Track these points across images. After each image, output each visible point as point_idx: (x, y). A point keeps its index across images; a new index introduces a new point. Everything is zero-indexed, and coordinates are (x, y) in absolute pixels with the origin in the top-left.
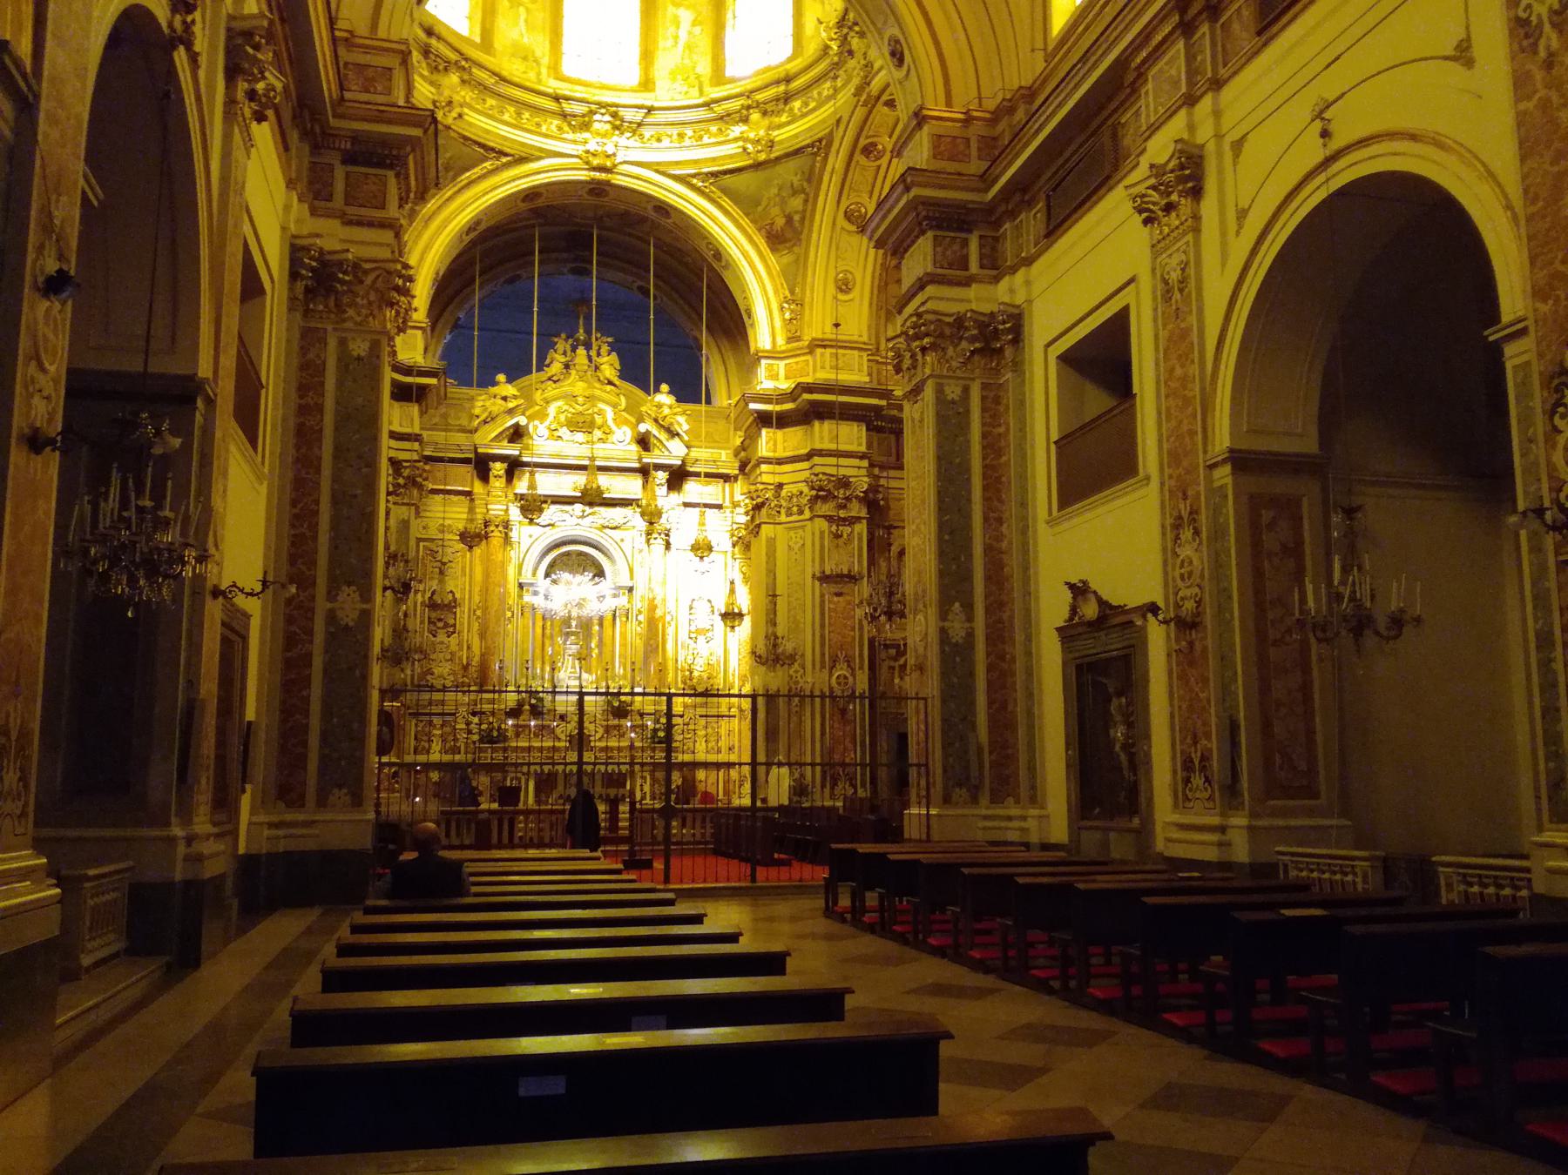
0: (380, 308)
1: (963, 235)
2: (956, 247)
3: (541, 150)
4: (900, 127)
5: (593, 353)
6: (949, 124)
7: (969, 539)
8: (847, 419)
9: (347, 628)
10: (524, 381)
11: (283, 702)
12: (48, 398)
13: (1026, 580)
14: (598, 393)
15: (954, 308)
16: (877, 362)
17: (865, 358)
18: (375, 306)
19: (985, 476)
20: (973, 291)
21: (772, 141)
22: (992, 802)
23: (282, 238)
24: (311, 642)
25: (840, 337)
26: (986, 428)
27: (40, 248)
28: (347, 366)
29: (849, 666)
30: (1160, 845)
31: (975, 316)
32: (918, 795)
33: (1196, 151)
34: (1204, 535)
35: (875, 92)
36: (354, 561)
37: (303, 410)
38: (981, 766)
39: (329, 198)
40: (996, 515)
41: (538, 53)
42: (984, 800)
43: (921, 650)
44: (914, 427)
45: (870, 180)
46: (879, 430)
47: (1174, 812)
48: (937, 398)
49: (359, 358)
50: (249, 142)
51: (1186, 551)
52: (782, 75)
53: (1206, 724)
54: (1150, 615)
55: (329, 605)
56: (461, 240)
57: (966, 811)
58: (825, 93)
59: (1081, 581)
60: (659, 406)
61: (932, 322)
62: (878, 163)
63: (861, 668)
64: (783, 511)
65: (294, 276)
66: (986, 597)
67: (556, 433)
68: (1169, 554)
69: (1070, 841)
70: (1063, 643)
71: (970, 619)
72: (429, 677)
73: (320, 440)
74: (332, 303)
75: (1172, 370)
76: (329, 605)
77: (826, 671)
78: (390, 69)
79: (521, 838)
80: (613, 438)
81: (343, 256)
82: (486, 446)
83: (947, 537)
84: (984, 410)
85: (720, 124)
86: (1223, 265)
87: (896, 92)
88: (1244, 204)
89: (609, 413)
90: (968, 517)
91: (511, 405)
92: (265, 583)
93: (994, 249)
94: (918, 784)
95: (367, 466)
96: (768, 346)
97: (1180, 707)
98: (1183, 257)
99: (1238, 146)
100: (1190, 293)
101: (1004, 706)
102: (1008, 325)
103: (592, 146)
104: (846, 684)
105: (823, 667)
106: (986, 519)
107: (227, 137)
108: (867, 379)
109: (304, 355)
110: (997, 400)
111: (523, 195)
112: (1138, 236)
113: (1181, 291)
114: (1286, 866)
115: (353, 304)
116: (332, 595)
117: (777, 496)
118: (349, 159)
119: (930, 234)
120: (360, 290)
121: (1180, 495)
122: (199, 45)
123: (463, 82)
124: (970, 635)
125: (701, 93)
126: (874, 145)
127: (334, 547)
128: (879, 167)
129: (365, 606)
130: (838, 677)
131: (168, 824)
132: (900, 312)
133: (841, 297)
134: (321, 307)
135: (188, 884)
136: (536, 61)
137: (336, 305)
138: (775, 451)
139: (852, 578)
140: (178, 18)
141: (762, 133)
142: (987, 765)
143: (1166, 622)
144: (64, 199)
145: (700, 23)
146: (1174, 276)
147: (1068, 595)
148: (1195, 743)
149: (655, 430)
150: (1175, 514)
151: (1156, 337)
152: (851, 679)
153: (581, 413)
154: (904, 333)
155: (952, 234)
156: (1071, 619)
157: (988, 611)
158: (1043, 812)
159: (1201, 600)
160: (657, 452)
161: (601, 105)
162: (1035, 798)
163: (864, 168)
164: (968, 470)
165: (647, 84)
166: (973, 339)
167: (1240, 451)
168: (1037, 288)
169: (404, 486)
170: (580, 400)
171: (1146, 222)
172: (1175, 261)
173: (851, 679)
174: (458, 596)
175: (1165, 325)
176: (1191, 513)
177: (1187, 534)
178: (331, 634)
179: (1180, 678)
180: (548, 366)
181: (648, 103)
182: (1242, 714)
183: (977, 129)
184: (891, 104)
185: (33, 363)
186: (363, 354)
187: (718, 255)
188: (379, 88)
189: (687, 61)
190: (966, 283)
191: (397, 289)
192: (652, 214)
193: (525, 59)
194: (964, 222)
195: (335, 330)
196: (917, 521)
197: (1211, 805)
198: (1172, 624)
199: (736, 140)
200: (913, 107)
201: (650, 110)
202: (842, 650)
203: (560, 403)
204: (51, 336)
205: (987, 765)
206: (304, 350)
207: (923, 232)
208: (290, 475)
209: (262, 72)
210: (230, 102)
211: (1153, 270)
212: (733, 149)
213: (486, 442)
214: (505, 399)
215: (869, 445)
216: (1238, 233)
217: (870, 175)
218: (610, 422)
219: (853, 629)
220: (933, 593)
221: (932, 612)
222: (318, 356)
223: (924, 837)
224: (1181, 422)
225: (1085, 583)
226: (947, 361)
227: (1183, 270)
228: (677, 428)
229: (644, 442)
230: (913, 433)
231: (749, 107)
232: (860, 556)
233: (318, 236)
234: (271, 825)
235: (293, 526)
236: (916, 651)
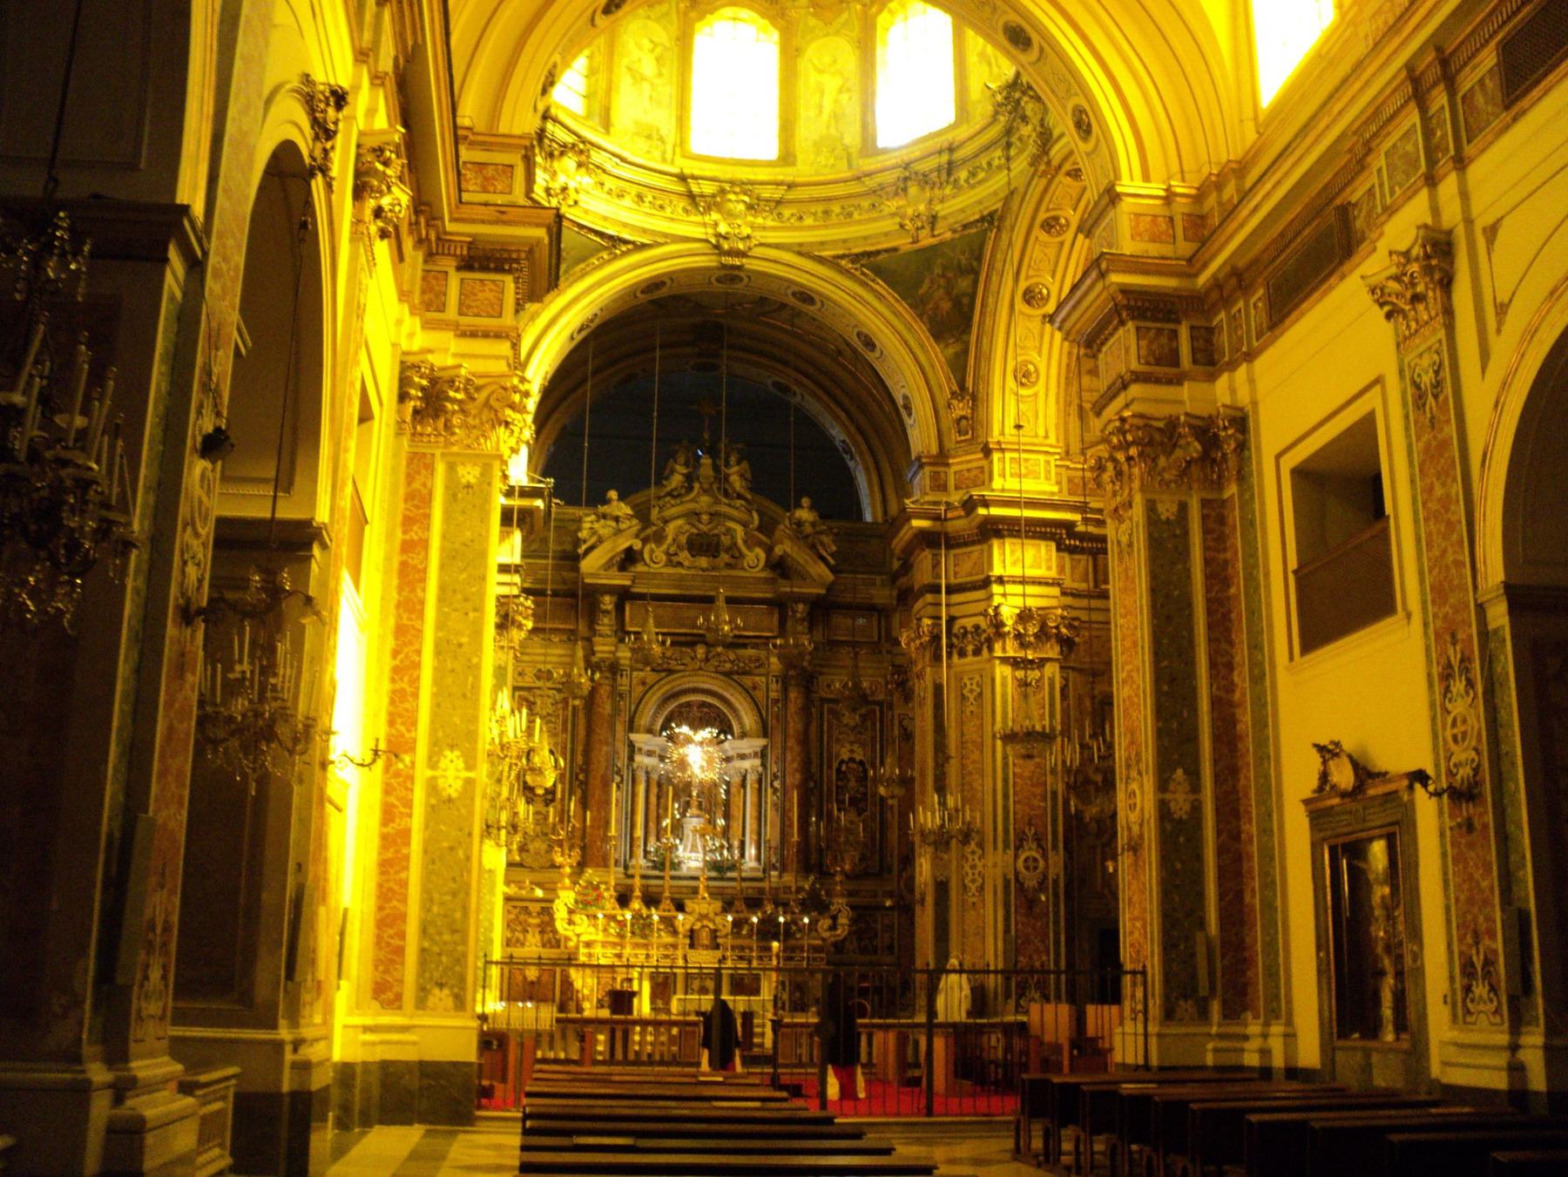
1: (1171, 326)
2: (1164, 340)
3: (666, 235)
4: (1087, 195)
6: (1151, 202)
7: (1194, 691)
8: (1033, 538)
9: (450, 800)
10: (640, 497)
11: (380, 886)
12: (198, 565)
13: (1262, 742)
14: (724, 509)
15: (1165, 411)
16: (1068, 468)
17: (1053, 463)
19: (1210, 612)
20: (1186, 391)
21: (934, 217)
23: (393, 356)
24: (410, 816)
25: (1023, 440)
26: (1211, 554)
27: (201, 406)
28: (454, 496)
29: (1039, 846)
30: (1436, 1070)
32: (1133, 1010)
33: (1442, 237)
35: (1055, 163)
36: (457, 720)
37: (407, 547)
39: (441, 308)
41: (664, 132)
43: (1136, 829)
44: (1121, 552)
45: (1052, 259)
46: (1072, 550)
47: (1451, 1029)
48: (1149, 517)
49: (468, 486)
50: (372, 261)
51: (1459, 707)
52: (946, 145)
53: (1490, 919)
54: (1418, 786)
55: (429, 773)
56: (572, 338)
57: (1192, 1030)
58: (996, 163)
59: (1332, 742)
61: (1138, 428)
62: (1060, 239)
63: (1055, 847)
65: (403, 397)
67: (675, 559)
68: (1439, 710)
69: (1323, 1064)
70: (1311, 820)
71: (1196, 788)
73: (423, 580)
75: (1431, 490)
76: (429, 773)
77: (1011, 852)
78: (511, 166)
79: (637, 1053)
83: (1165, 688)
84: (1206, 531)
85: (873, 199)
86: (1483, 372)
87: (1084, 164)
88: (1503, 297)
90: (1191, 663)
92: (376, 752)
93: (1209, 341)
94: (1133, 996)
95: (475, 610)
97: (1457, 900)
98: (1436, 357)
99: (1492, 231)
100: (1446, 399)
101: (1239, 895)
103: (723, 228)
104: (1036, 868)
105: (1006, 846)
106: (1213, 665)
107: (353, 258)
108: (1055, 489)
109: (409, 484)
110: (1222, 520)
111: (643, 285)
112: (1379, 332)
113: (1436, 397)
116: (433, 763)
118: (467, 265)
119: (1130, 325)
121: (1448, 638)
122: (335, 171)
123: (580, 165)
124: (1197, 809)
125: (850, 166)
126: (1056, 219)
127: (437, 706)
128: (1062, 244)
130: (1026, 860)
131: (274, 1026)
132: (1098, 414)
133: (1023, 392)
134: (429, 430)
135: (294, 1094)
136: (662, 140)
137: (446, 425)
139: (1046, 737)
140: (319, 145)
141: (922, 208)
143: (1437, 794)
144: (220, 353)
145: (848, 90)
146: (1427, 379)
147: (1315, 760)
148: (1477, 943)
150: (1443, 661)
151: (1410, 446)
152: (1041, 864)
154: (1105, 440)
155: (1159, 325)
156: (1320, 789)
157: (1217, 778)
159: (1479, 765)
161: (732, 183)
162: (1278, 1008)
163: (1046, 245)
164: (1190, 605)
165: (787, 158)
168: (1262, 386)
170: (705, 517)
171: (1389, 316)
172: (1426, 362)
173: (1041, 864)
175: (1418, 440)
176: (1462, 661)
177: (1458, 686)
178: (433, 807)
179: (1455, 861)
180: (667, 479)
181: (789, 179)
183: (1181, 207)
184: (1076, 174)
185: (189, 529)
188: (499, 187)
189: (833, 131)
190: (1177, 381)
191: (512, 406)
192: (792, 301)
193: (649, 137)
194: (1170, 312)
195: (443, 455)
196: (1128, 668)
197: (1498, 1019)
198: (1445, 796)
199: (893, 215)
200: (1104, 183)
201: (791, 186)
202: (1030, 824)
203: (680, 522)
204: (205, 499)
206: (410, 478)
207: (1122, 323)
208: (392, 622)
209: (389, 188)
210: (358, 221)
211: (1401, 372)
212: (890, 225)
215: (1061, 569)
216: (1499, 331)
217: (1051, 252)
219: (1044, 799)
220: (1149, 755)
221: (1149, 783)
222: (424, 485)
223: (1141, 1061)
224: (1444, 552)
225: (1337, 744)
227: (1437, 373)
229: (780, 567)
230: (1121, 560)
231: (906, 179)
232: (1052, 705)
233: (430, 351)
234: (367, 1029)
235: (393, 680)
236: (1129, 829)
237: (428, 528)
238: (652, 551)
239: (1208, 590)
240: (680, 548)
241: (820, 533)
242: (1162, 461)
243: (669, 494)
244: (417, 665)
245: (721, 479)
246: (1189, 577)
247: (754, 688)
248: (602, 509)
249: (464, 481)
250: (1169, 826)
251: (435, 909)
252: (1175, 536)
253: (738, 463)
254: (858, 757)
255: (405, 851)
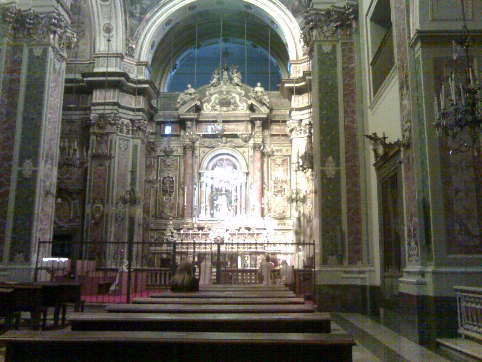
0: (47, 34)
5: (230, 73)
9: (27, 179)
10: (201, 88)
18: (45, 34)
22: (350, 263)
26: (345, 65)
31: (335, 9)
34: (410, 88)
38: (343, 244)
40: (351, 110)
42: (346, 262)
49: (38, 57)
55: (19, 169)
56: (164, 29)
57: (334, 269)
60: (257, 92)
64: (302, 132)
66: (346, 153)
71: (338, 164)
72: (162, 214)
74: (26, 33)
76: (19, 169)
80: (240, 108)
81: (28, 12)
82: (183, 115)
84: (343, 56)
89: (237, 98)
90: (336, 112)
91: (193, 97)
95: (39, 105)
96: (295, 59)
102: (350, 10)
106: (346, 111)
114: (460, 298)
115: (36, 33)
116: (20, 165)
117: (300, 125)
120: (40, 26)
124: (338, 173)
127: (23, 142)
129: (35, 168)
134: (21, 35)
138: (299, 105)
142: (347, 243)
149: (254, 103)
153: (224, 99)
158: (372, 269)
160: (257, 112)
164: (336, 87)
166: (336, 21)
167: (424, 32)
169: (136, 131)
170: (225, 93)
174: (174, 179)
178: (20, 182)
182: (430, 200)
186: (39, 55)
187: (273, 22)
203: (217, 95)
205: (347, 243)
213: (183, 113)
214: (191, 94)
218: (238, 102)
222: (19, 57)
226: (323, 33)
228: (264, 101)
229: (252, 108)
237: (19, 74)
238: (206, 106)
239: (344, 80)
240: (217, 104)
241: (264, 95)
242: (325, 28)
243: (212, 85)
244: (14, 127)
245: (231, 79)
246: (336, 76)
247: (244, 152)
248: (186, 91)
249: (36, 55)
250: (325, 181)
251: (19, 222)
252: (330, 59)
253: (237, 72)
254: (170, 176)
255: (6, 199)
